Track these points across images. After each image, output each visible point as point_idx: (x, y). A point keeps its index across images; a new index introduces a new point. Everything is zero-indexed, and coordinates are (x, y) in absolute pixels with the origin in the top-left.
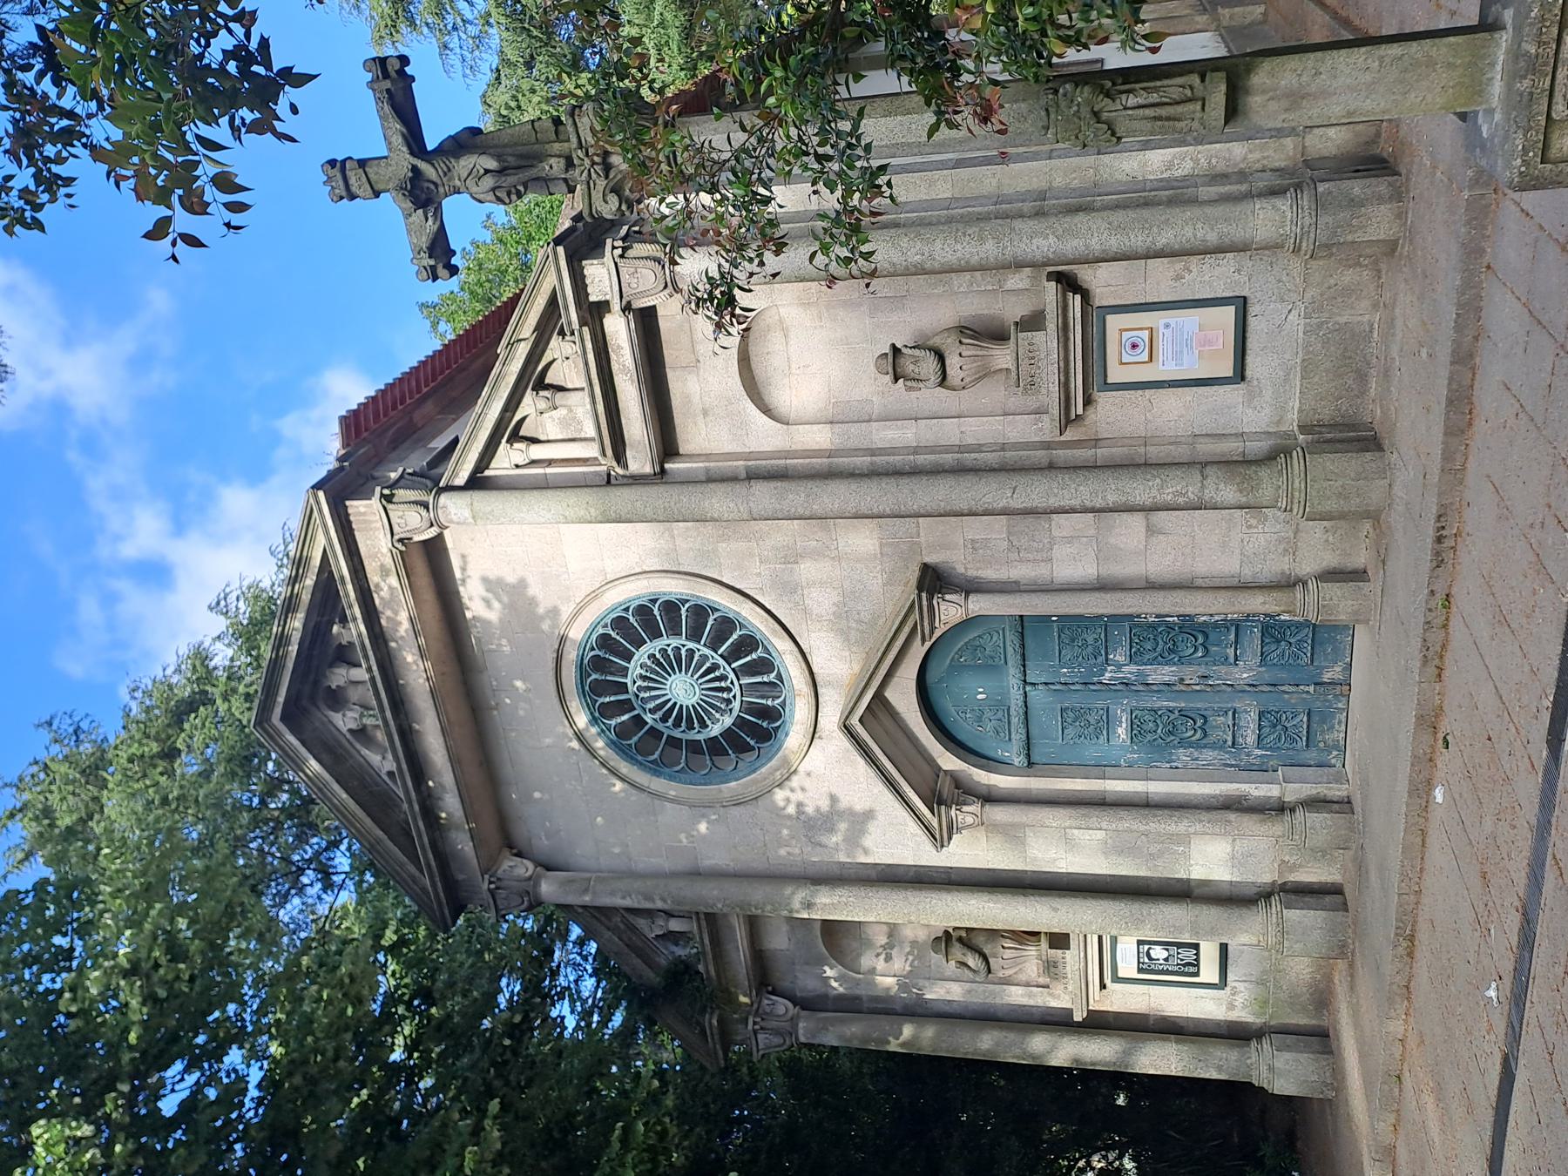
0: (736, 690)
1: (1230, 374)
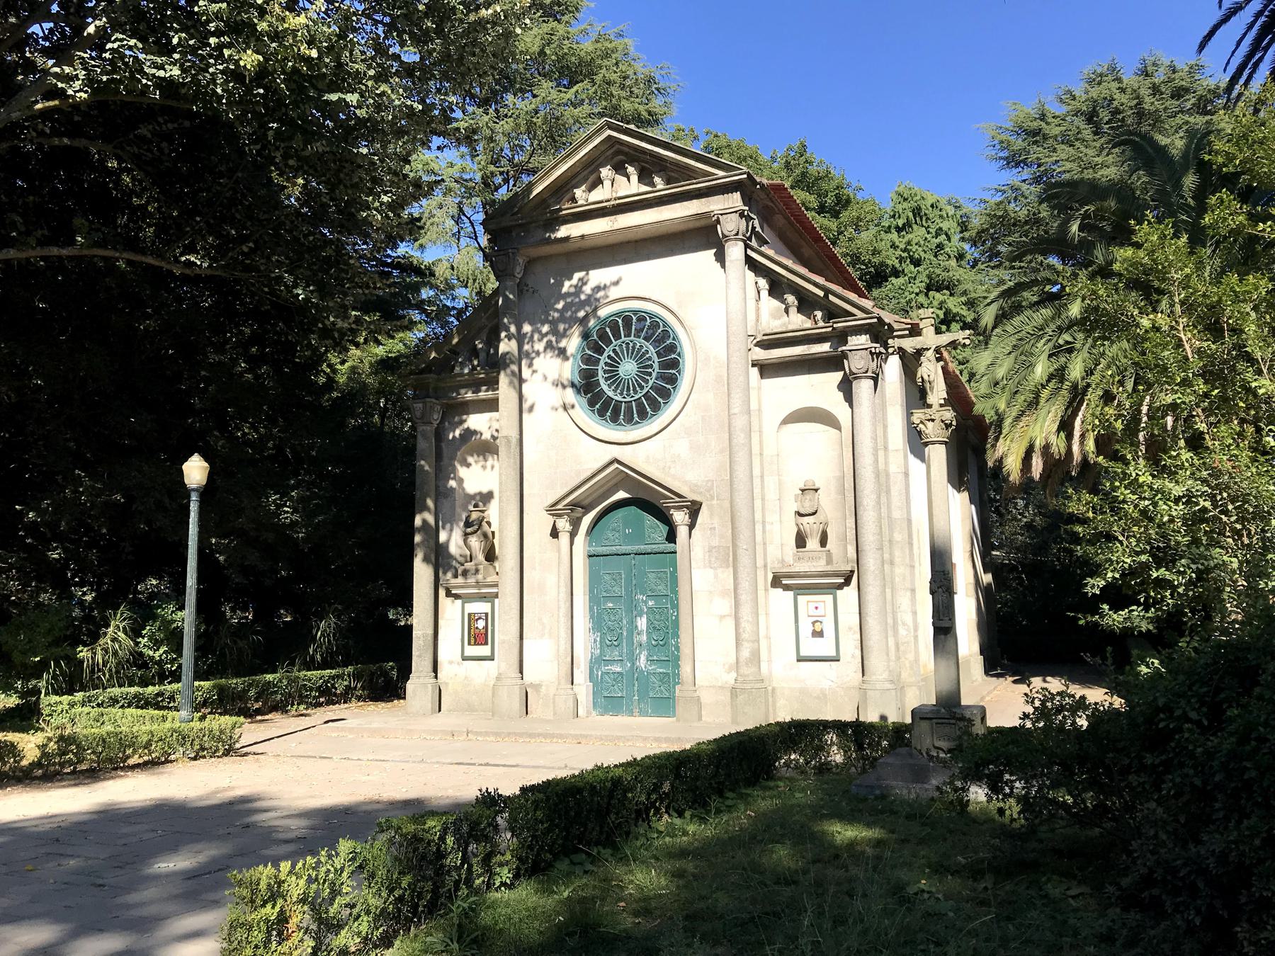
0: (628, 399)
1: (802, 654)
